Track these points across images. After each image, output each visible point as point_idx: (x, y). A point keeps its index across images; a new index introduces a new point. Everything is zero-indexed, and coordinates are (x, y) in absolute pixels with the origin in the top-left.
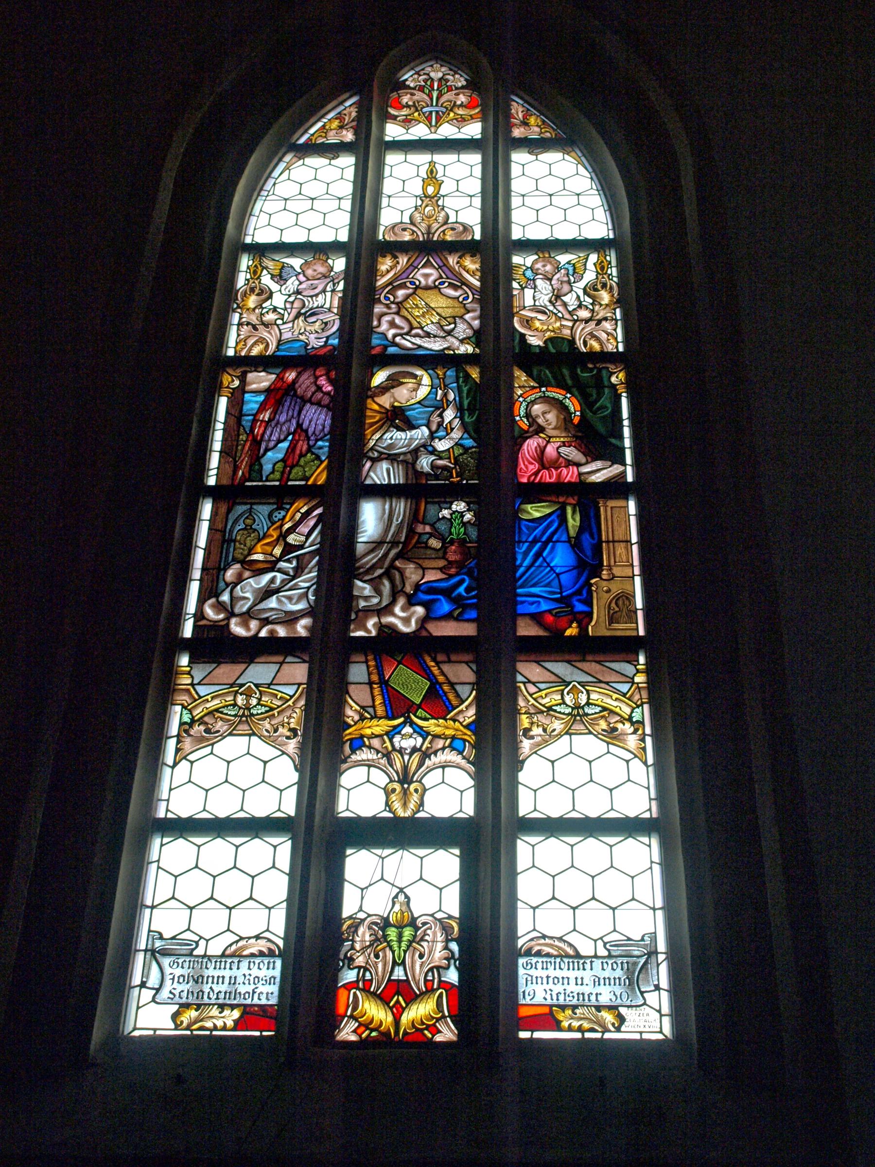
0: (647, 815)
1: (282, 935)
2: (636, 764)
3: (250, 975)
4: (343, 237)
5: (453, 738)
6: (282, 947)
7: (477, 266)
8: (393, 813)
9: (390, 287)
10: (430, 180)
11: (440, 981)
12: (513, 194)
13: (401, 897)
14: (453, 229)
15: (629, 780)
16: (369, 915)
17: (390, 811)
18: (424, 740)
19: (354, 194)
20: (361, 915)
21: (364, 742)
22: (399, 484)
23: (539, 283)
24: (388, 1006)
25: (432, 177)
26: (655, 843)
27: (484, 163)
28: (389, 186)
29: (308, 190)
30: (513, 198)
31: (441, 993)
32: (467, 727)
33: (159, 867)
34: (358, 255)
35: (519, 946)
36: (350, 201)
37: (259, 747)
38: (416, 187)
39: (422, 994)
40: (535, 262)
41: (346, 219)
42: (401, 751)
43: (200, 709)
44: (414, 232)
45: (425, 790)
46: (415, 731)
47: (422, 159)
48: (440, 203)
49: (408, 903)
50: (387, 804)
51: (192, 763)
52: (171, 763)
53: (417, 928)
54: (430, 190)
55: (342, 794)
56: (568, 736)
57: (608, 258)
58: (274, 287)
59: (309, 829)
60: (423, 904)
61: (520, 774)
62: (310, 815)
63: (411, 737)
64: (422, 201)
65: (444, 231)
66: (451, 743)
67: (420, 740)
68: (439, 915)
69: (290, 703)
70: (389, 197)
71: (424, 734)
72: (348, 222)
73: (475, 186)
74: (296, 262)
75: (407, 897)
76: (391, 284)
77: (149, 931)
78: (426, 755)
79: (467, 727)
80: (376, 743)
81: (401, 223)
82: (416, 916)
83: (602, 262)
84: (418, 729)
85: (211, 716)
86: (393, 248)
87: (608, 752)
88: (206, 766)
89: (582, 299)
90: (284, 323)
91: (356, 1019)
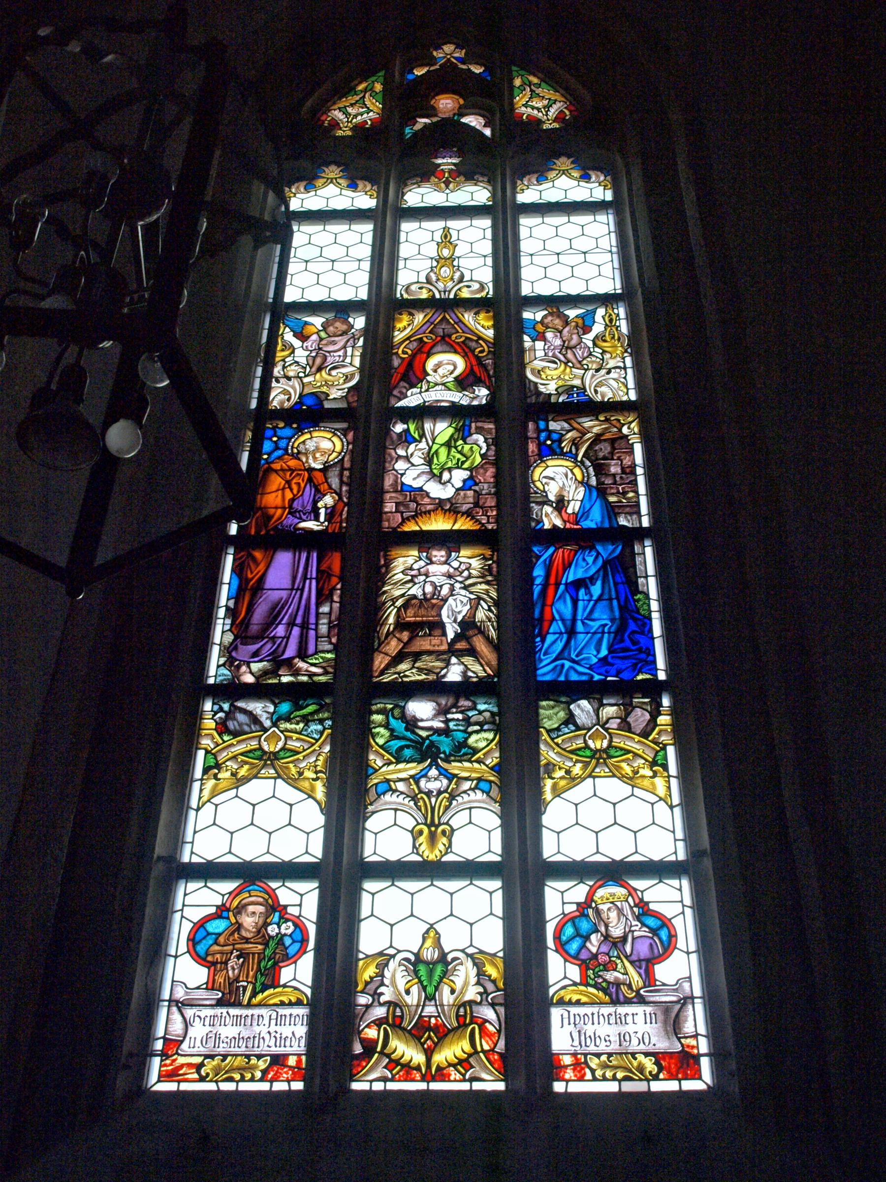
0: (673, 858)
1: (310, 984)
2: (661, 807)
3: (276, 1032)
4: (363, 295)
5: (479, 780)
6: (309, 996)
7: (491, 323)
8: (422, 856)
9: (407, 342)
10: (445, 245)
11: (472, 1017)
12: (522, 254)
13: (432, 934)
14: (469, 287)
15: (654, 823)
16: (399, 951)
17: (418, 854)
18: (450, 782)
19: (373, 257)
20: (391, 951)
21: (390, 786)
22: (449, 298)
23: (549, 335)
24: (419, 1041)
25: (446, 238)
26: (685, 883)
27: (494, 227)
28: (405, 250)
29: (329, 253)
30: (522, 258)
31: (474, 1029)
32: (492, 768)
33: (182, 917)
34: (377, 312)
35: (551, 995)
36: (369, 263)
37: (284, 789)
38: (431, 250)
39: (454, 1030)
40: (545, 317)
41: (365, 278)
42: (429, 794)
43: (225, 754)
44: (430, 290)
45: (453, 831)
46: (441, 774)
47: (437, 225)
48: (455, 263)
49: (439, 938)
50: (414, 846)
51: (216, 805)
52: (195, 807)
53: (447, 964)
54: (446, 253)
55: (369, 838)
56: (591, 780)
57: (616, 311)
58: (297, 343)
59: (337, 872)
60: (454, 939)
61: (544, 817)
62: (338, 861)
63: (436, 779)
64: (438, 262)
65: (459, 289)
66: (477, 784)
67: (445, 782)
68: (470, 951)
69: (316, 747)
70: (405, 259)
71: (451, 777)
72: (367, 281)
73: (486, 247)
74: (317, 321)
75: (437, 933)
76: (408, 338)
77: (173, 981)
78: (452, 797)
79: (492, 768)
80: (401, 786)
81: (418, 282)
82: (446, 951)
83: (610, 315)
84: (442, 771)
85: (234, 760)
86: (413, 305)
87: (633, 795)
88: (232, 810)
89: (592, 350)
90: (306, 376)
91: (388, 1056)
